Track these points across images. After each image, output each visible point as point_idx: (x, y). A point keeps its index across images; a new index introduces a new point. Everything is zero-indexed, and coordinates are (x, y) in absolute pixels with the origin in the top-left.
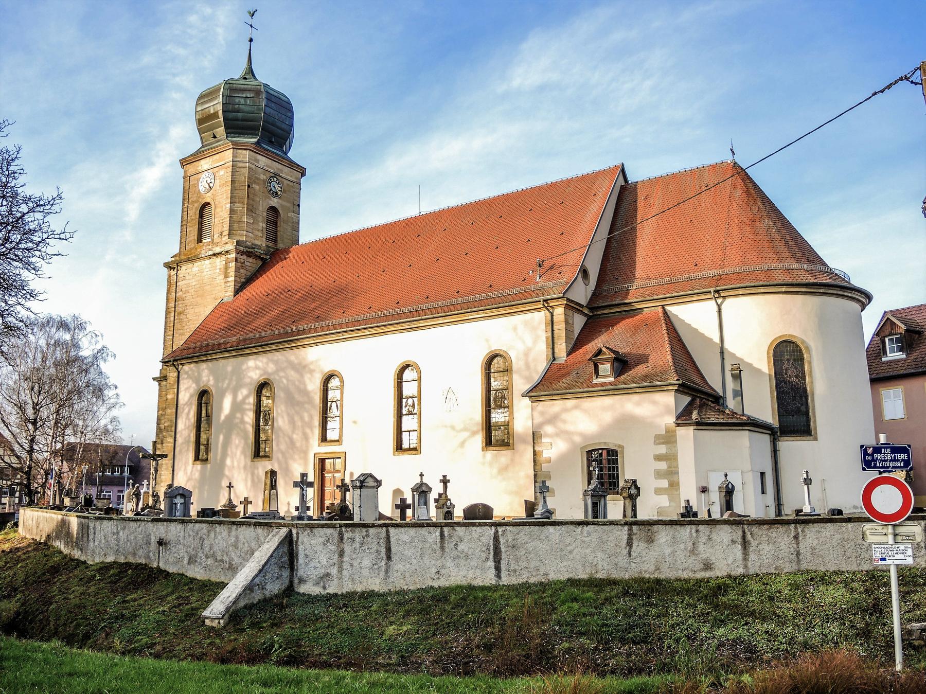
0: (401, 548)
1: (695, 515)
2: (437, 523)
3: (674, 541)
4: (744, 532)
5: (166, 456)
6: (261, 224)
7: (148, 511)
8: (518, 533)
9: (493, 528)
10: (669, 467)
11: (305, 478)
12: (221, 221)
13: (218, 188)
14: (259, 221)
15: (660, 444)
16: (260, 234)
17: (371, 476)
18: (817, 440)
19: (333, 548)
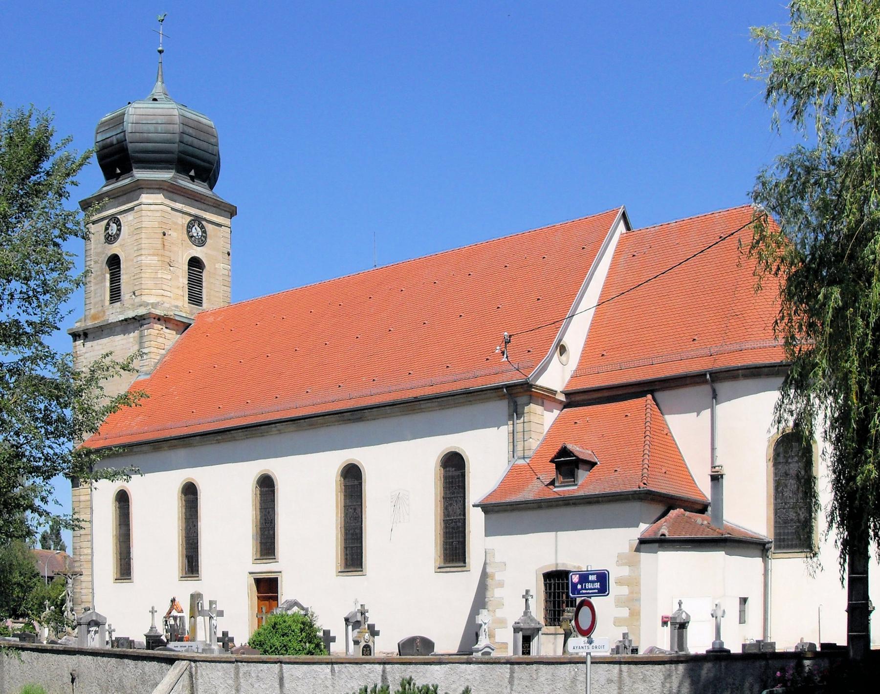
0: (294, 685)
1: (635, 651)
2: (678, 657)
3: (553, 679)
4: (621, 671)
5: (474, 506)
6: (181, 280)
7: (66, 639)
8: (405, 670)
9: (382, 666)
10: (631, 592)
11: (214, 606)
12: (133, 278)
13: (127, 237)
14: (178, 276)
15: (623, 565)
16: (180, 292)
17: (296, 604)
18: (223, 611)
19: (230, 682)
